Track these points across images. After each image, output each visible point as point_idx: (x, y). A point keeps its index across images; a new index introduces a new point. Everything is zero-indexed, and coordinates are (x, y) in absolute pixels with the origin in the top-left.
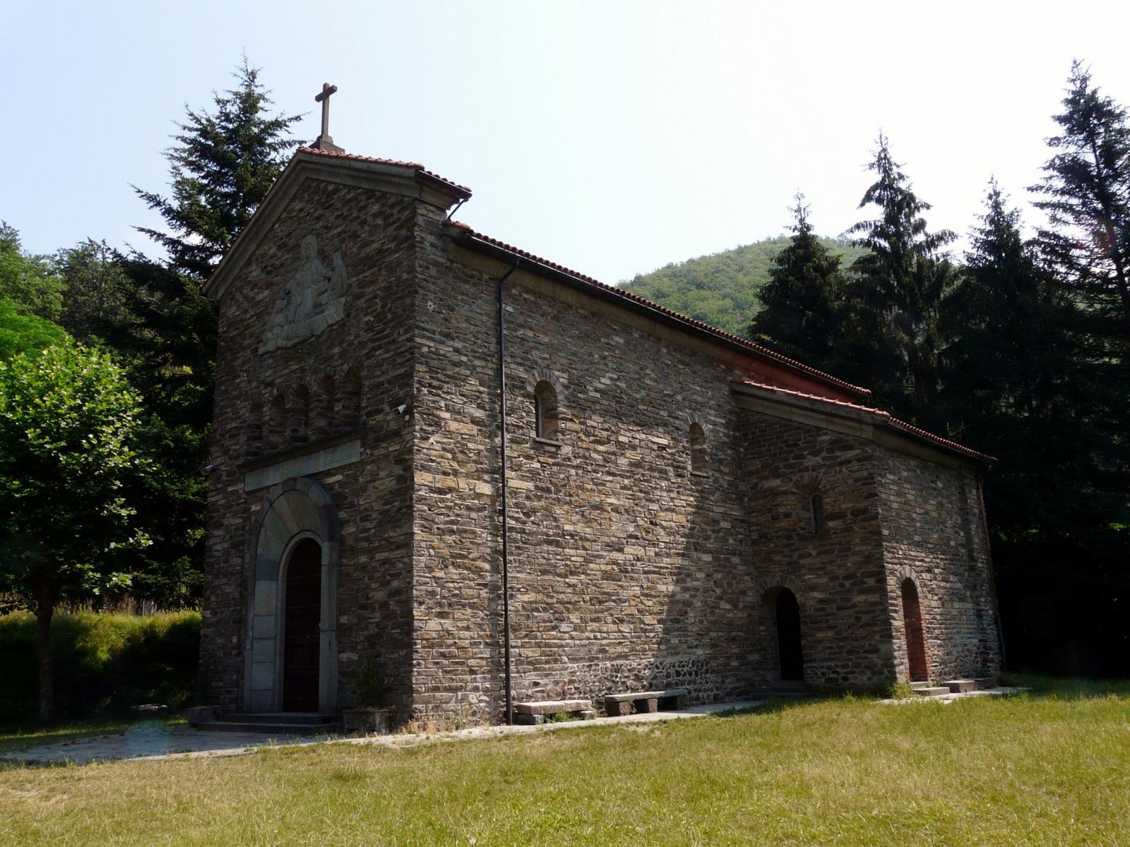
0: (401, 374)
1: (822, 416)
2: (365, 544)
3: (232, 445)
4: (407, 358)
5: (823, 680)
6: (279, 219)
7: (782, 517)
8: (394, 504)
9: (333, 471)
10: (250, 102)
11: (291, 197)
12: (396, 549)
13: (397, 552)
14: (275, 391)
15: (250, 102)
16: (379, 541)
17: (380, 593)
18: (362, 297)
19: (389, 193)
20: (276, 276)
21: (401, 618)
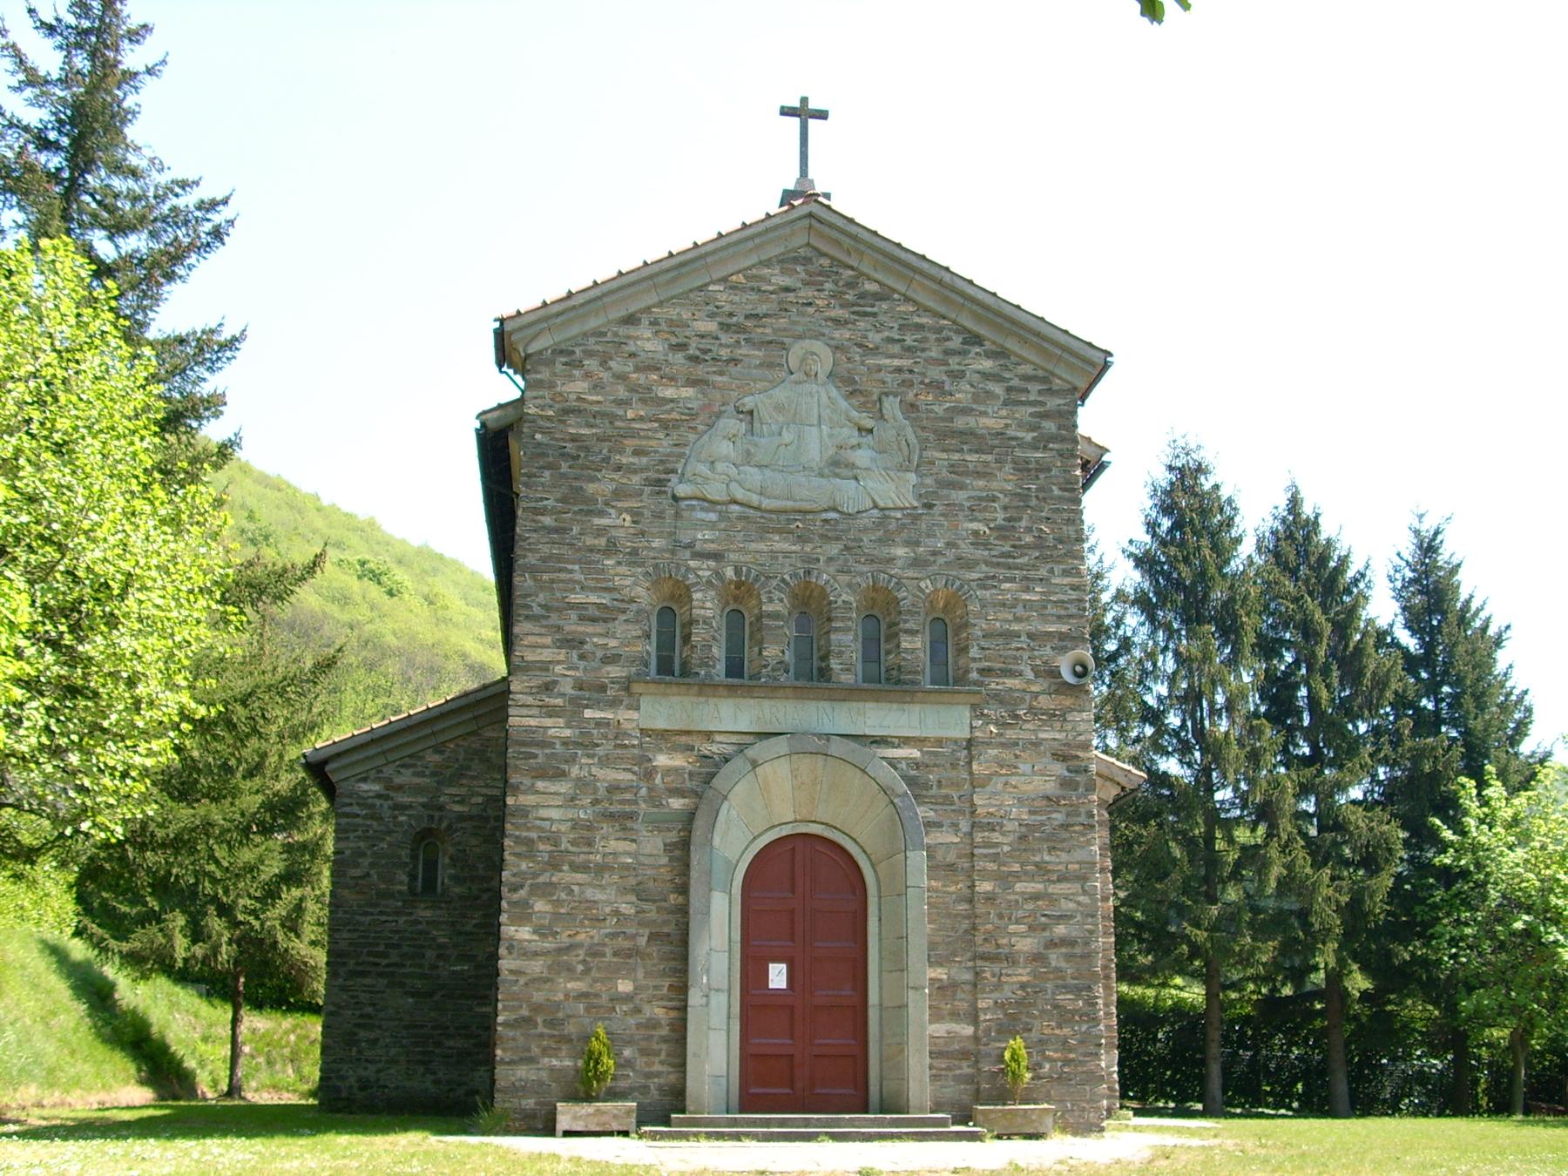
0: (1061, 633)
1: (645, 285)
2: (992, 866)
3: (595, 635)
4: (1070, 612)
5: (440, 1075)
6: (724, 280)
7: (824, 665)
8: (1054, 816)
9: (896, 741)
10: (1294, 503)
11: (763, 258)
12: (1059, 880)
13: (1059, 886)
14: (730, 573)
15: (1294, 503)
16: (1022, 865)
17: (1029, 940)
18: (961, 489)
19: (1017, 355)
20: (721, 373)
21: (1073, 978)
